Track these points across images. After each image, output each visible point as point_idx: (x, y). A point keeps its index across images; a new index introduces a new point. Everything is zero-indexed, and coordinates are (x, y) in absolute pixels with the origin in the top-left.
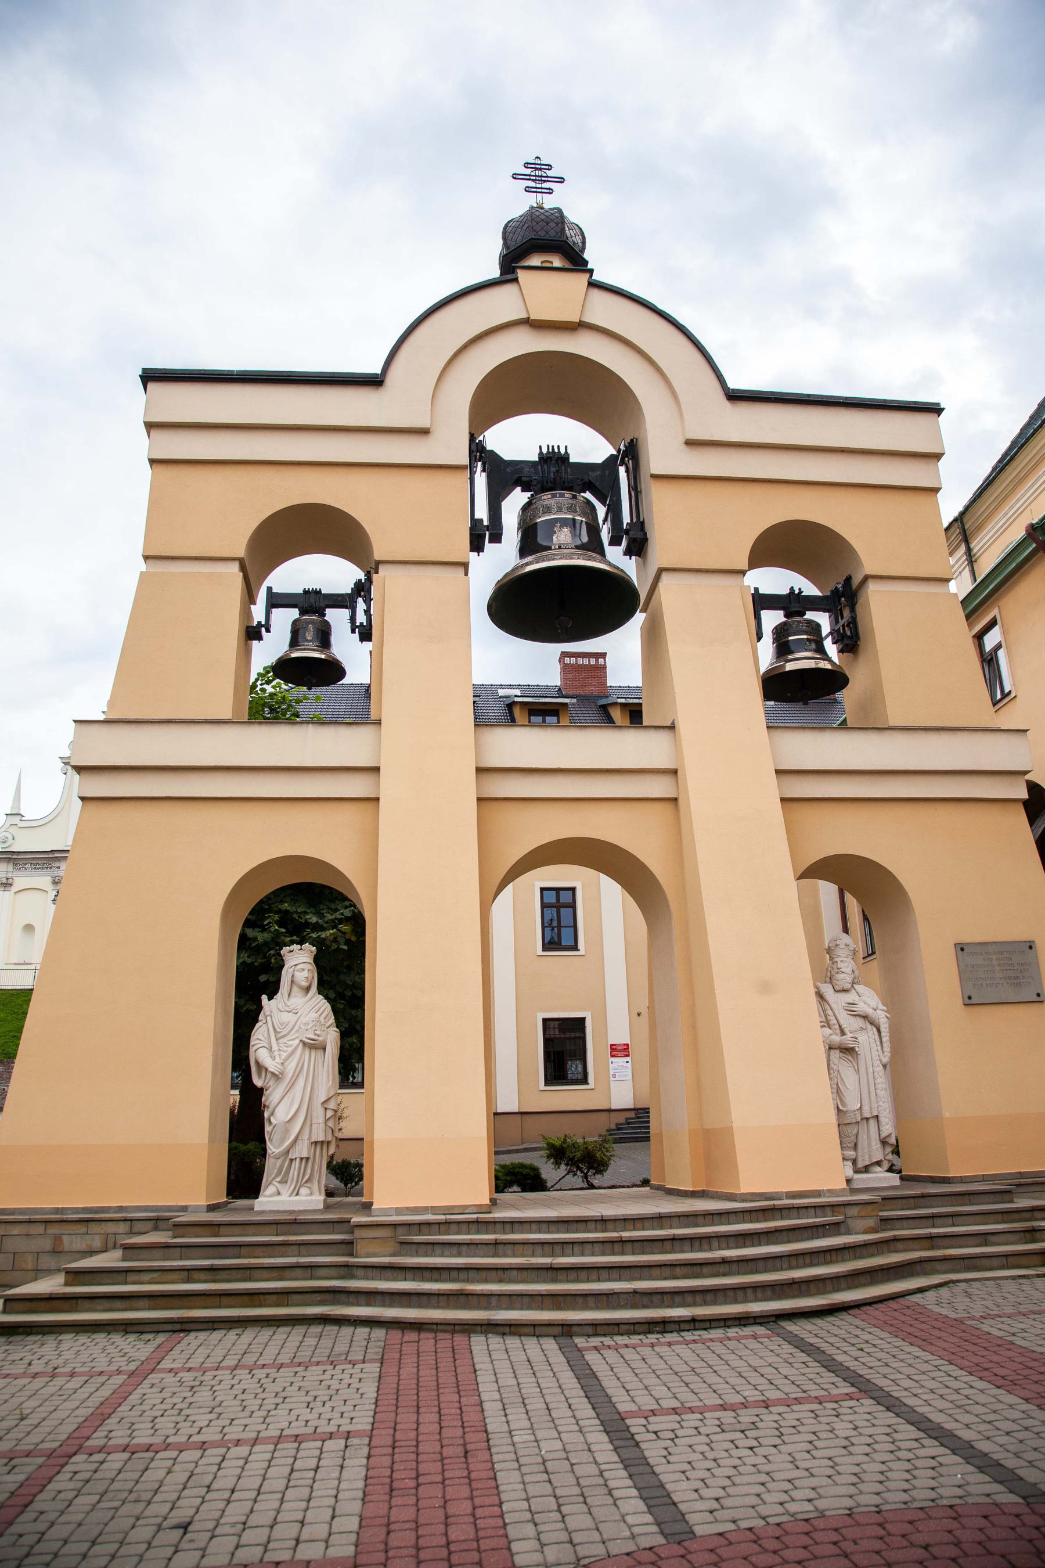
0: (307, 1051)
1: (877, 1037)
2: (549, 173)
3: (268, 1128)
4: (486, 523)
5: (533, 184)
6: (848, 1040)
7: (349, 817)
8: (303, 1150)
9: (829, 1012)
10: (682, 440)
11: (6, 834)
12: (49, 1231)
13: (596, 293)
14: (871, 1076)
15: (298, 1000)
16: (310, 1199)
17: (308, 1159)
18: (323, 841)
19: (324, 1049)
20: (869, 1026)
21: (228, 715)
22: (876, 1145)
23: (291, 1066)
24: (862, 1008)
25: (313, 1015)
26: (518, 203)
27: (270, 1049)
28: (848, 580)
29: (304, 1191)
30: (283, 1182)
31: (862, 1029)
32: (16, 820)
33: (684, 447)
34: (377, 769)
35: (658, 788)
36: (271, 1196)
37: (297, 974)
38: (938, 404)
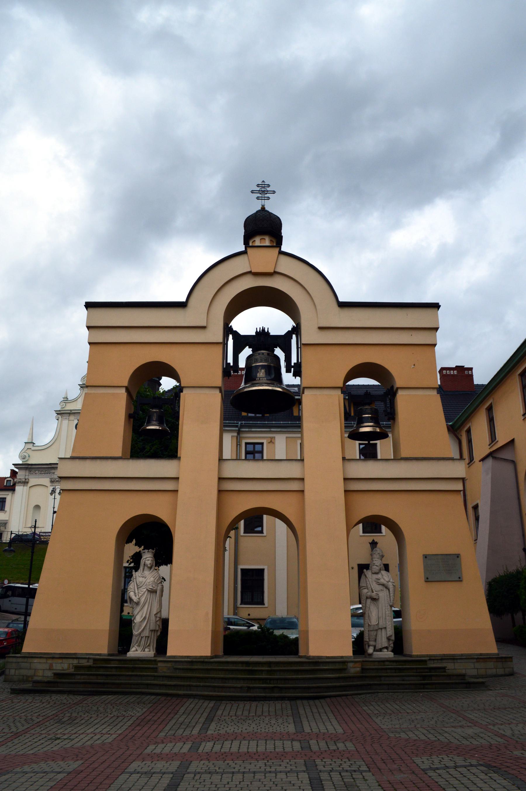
0: (149, 593)
1: (388, 594)
2: (268, 189)
3: (133, 624)
4: (232, 364)
5: (261, 196)
6: (374, 595)
7: (166, 498)
8: (146, 633)
9: (368, 582)
10: (316, 327)
11: (25, 454)
12: (48, 662)
13: (283, 258)
14: (384, 611)
15: (147, 573)
16: (149, 653)
17: (148, 637)
18: (156, 508)
19: (156, 592)
20: (385, 589)
21: (120, 454)
22: (384, 640)
23: (143, 600)
24: (382, 581)
25: (152, 579)
26: (255, 207)
27: (135, 593)
28: (392, 387)
29: (147, 650)
30: (139, 646)
31: (382, 590)
32: (30, 446)
33: (317, 330)
34: (177, 479)
35: (295, 486)
36: (134, 651)
37: (146, 562)
38: (438, 303)
